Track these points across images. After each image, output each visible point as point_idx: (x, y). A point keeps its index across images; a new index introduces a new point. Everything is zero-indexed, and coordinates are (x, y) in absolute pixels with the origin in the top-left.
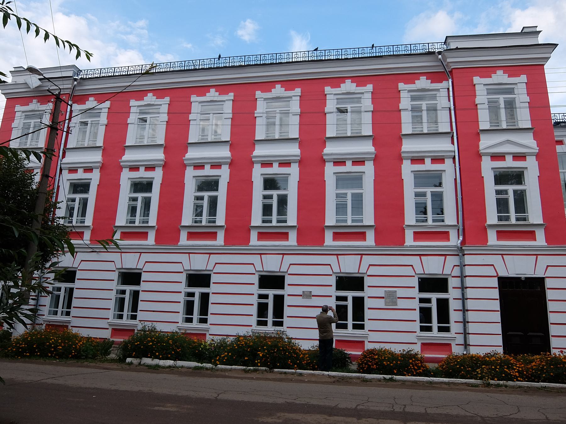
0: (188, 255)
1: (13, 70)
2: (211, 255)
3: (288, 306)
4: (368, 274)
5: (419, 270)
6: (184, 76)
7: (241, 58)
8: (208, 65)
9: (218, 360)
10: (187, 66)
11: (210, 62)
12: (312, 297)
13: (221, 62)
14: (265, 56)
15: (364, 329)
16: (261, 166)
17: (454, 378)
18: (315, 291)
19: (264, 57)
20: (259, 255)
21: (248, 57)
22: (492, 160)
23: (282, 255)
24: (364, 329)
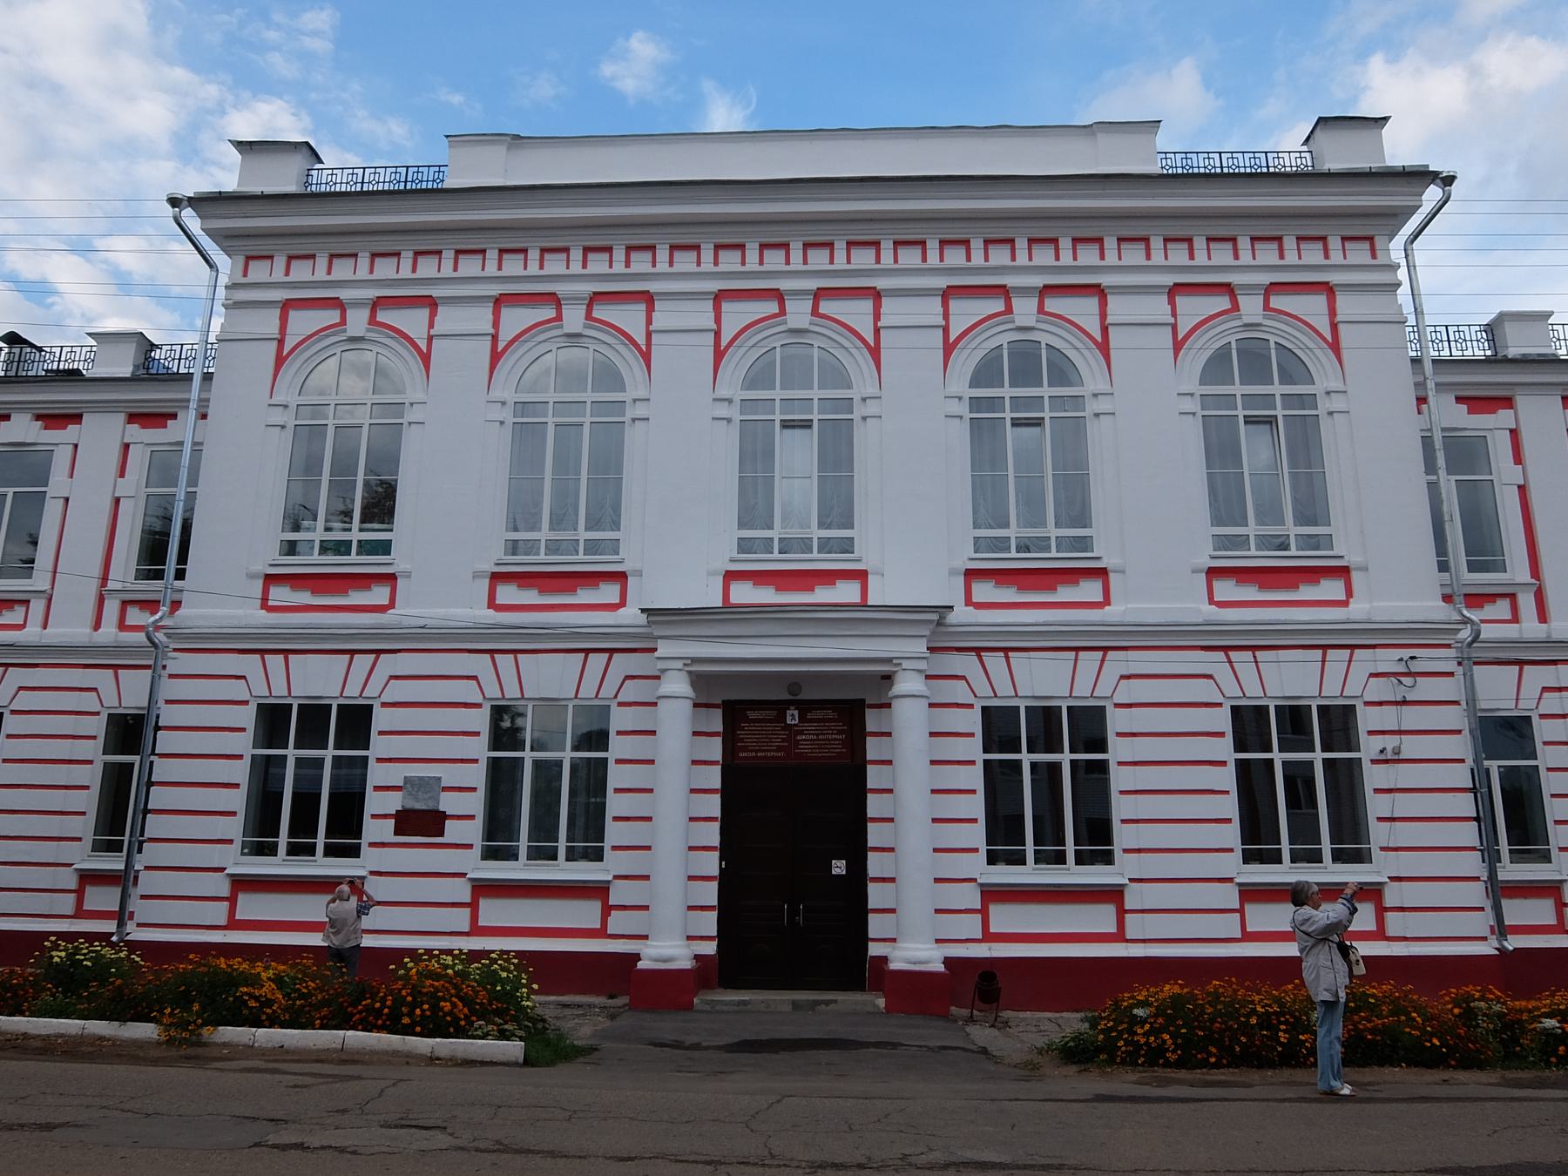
0: (511, 656)
1: (227, 176)
2: (590, 655)
3: (1122, 792)
4: (1367, 699)
5: (111, 700)
6: (870, 196)
7: (439, 172)
8: (387, 184)
9: (160, 981)
10: (369, 182)
11: (416, 174)
12: (401, 784)
13: (339, 181)
14: (421, 169)
15: (1065, 864)
16: (1563, 403)
17: (73, 1017)
18: (1412, 747)
19: (330, 177)
20: (1222, 653)
21: (373, 170)
22: (1457, 403)
23: (1321, 651)
24: (1065, 864)
